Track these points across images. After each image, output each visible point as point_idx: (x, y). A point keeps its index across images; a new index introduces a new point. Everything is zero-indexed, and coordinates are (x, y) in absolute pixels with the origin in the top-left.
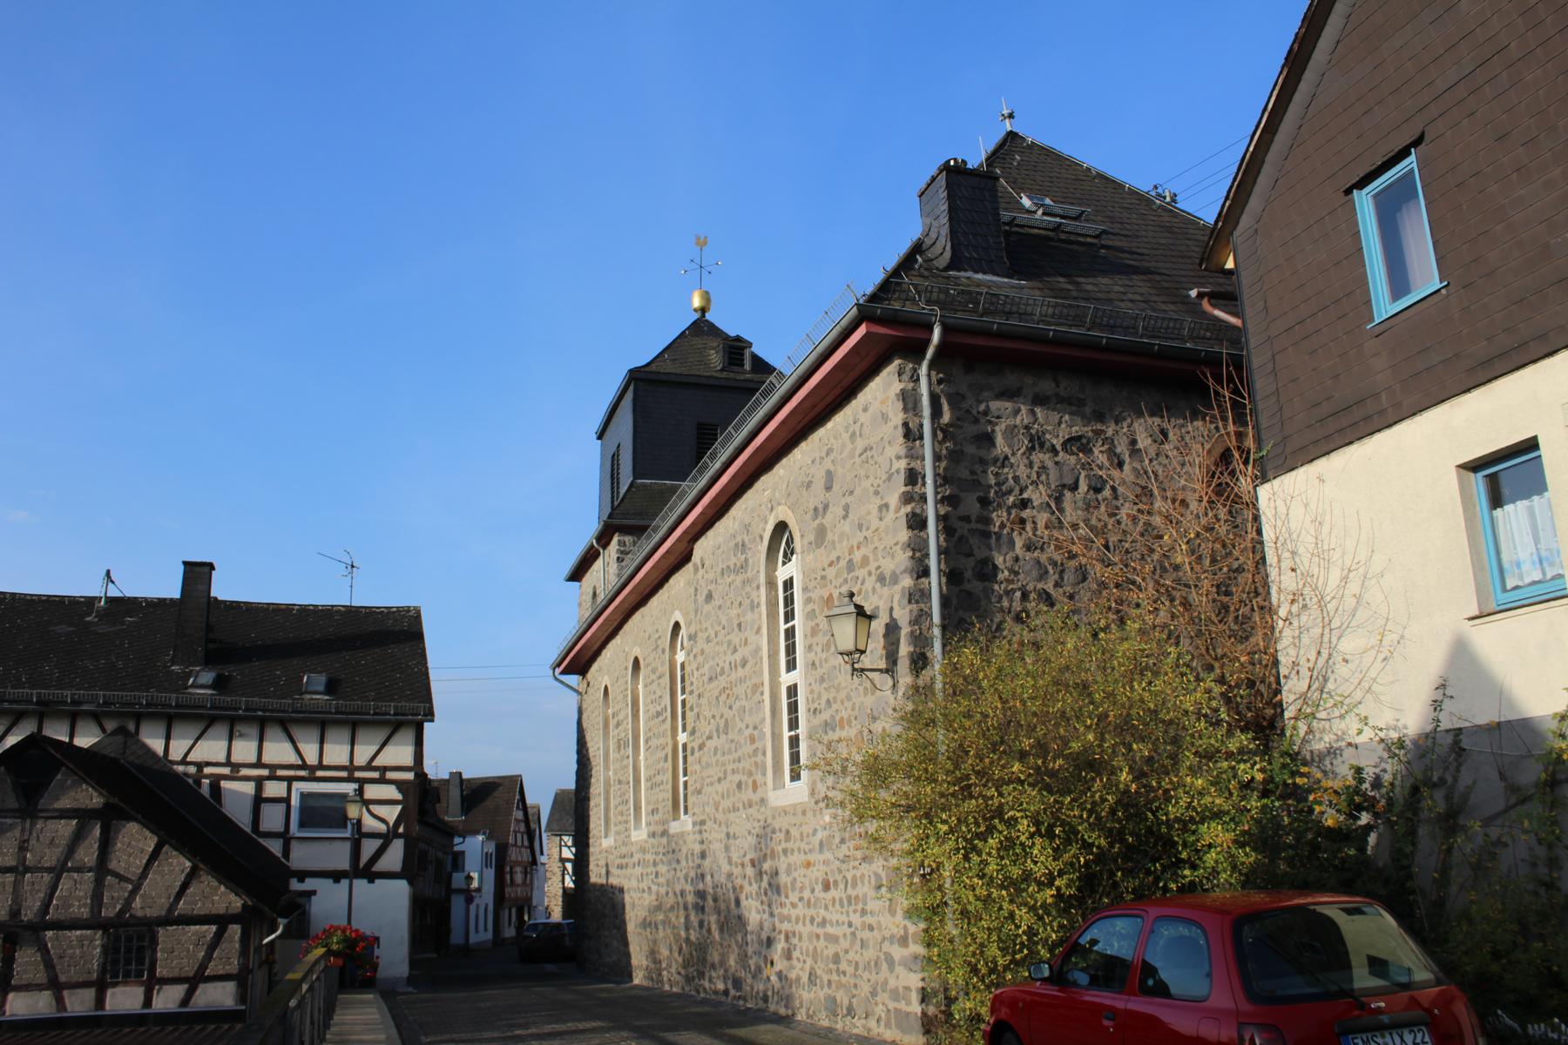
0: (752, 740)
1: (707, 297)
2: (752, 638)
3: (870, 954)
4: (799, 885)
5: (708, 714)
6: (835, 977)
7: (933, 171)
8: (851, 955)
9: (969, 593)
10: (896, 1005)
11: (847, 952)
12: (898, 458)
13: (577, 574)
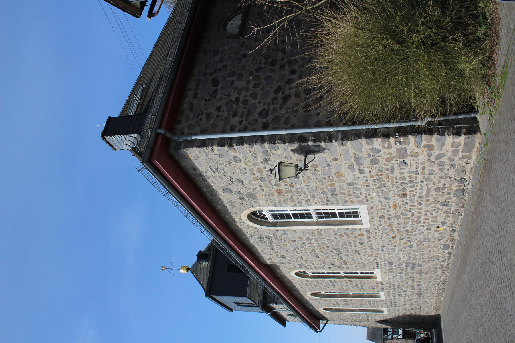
0: (341, 236)
1: (182, 267)
2: (298, 234)
3: (436, 168)
4: (404, 211)
5: (332, 258)
6: (446, 190)
7: (104, 142)
8: (436, 181)
9: (273, 120)
10: (460, 152)
11: (434, 183)
12: (213, 150)
13: (282, 321)
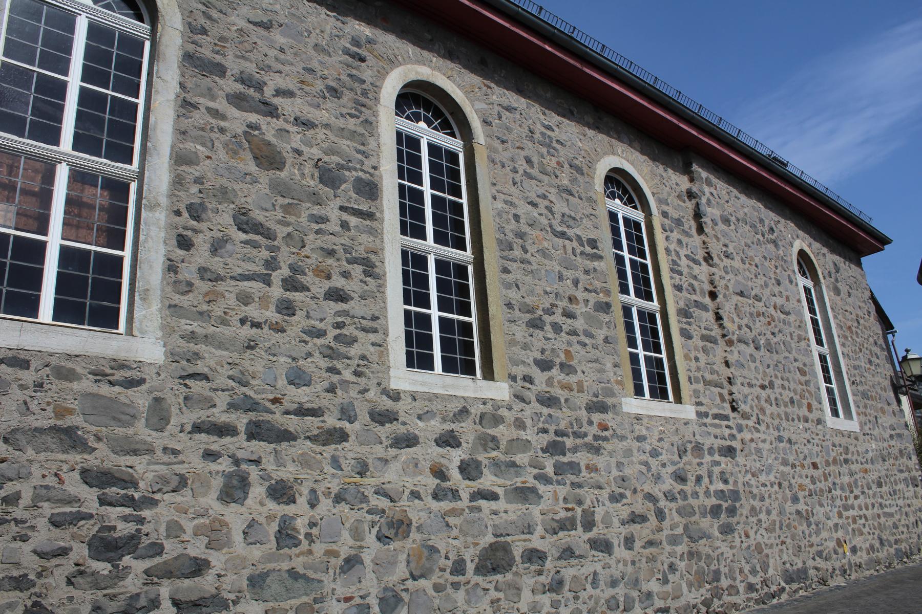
8: (903, 522)
11: (900, 521)
